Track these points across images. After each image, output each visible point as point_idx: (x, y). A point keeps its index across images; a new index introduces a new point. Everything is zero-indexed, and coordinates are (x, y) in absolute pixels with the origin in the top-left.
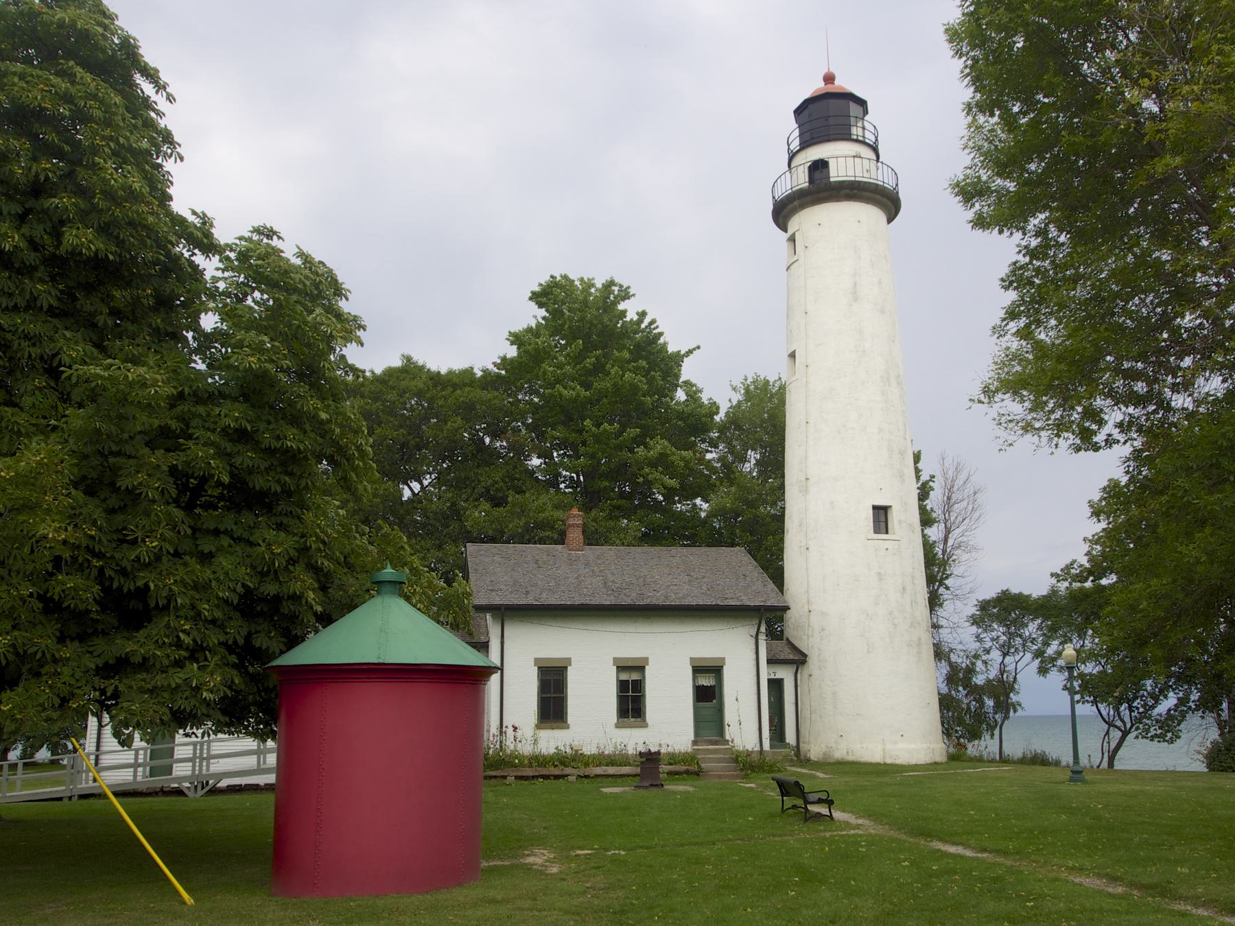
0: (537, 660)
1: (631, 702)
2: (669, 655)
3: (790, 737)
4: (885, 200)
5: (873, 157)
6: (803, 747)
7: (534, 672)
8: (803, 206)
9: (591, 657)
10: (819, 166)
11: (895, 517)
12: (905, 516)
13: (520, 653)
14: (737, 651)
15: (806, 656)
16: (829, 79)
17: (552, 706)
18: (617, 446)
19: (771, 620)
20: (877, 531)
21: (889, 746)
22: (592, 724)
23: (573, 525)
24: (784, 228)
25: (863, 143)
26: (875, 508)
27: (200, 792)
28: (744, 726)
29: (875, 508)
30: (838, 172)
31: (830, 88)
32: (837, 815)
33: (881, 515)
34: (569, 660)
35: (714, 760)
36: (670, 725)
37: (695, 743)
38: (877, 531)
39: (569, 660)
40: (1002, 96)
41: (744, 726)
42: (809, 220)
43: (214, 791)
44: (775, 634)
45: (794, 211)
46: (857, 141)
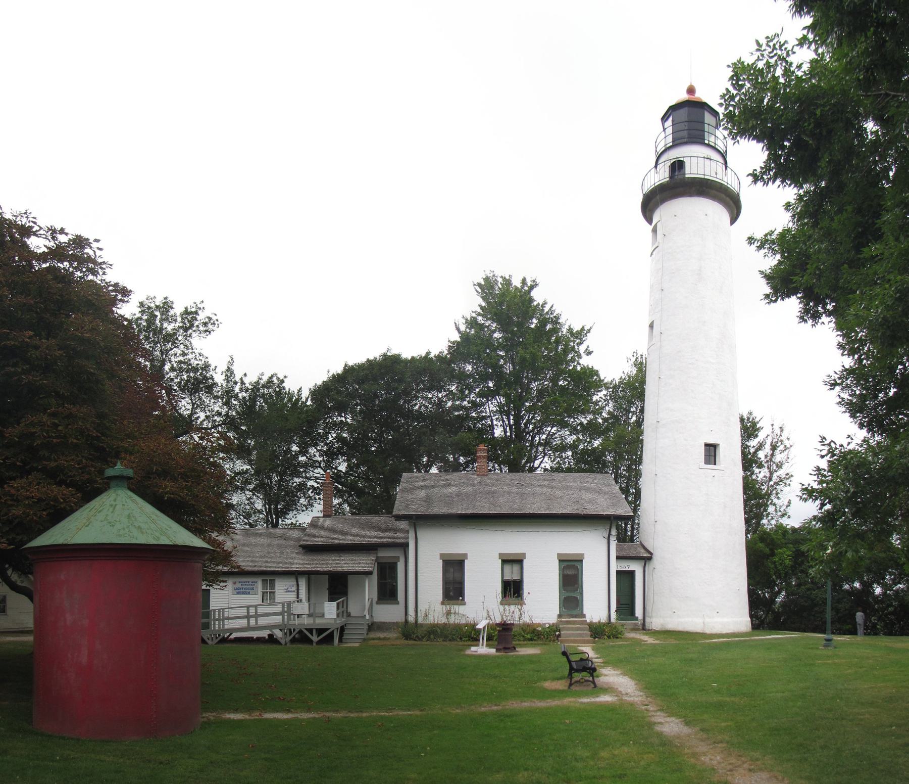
0: (442, 555)
1: (512, 590)
2: (542, 552)
3: (639, 612)
4: (728, 199)
5: (721, 160)
6: (647, 620)
7: (440, 564)
8: (663, 201)
9: (483, 553)
10: (677, 166)
11: (722, 453)
12: (730, 454)
13: (429, 552)
14: (595, 552)
15: (651, 554)
16: (691, 90)
17: (454, 590)
18: (512, 397)
19: (624, 529)
20: (707, 462)
21: (707, 620)
22: (482, 605)
23: (480, 457)
24: (650, 221)
25: (714, 148)
26: (706, 445)
27: (216, 641)
28: (597, 604)
29: (706, 445)
30: (692, 170)
31: (691, 98)
32: (610, 676)
33: (711, 452)
34: (465, 555)
35: (572, 629)
36: (541, 605)
37: (560, 616)
38: (707, 462)
39: (465, 555)
40: (187, 372)
41: (597, 604)
42: (667, 212)
43: (224, 641)
44: (623, 538)
45: (656, 206)
46: (709, 145)
